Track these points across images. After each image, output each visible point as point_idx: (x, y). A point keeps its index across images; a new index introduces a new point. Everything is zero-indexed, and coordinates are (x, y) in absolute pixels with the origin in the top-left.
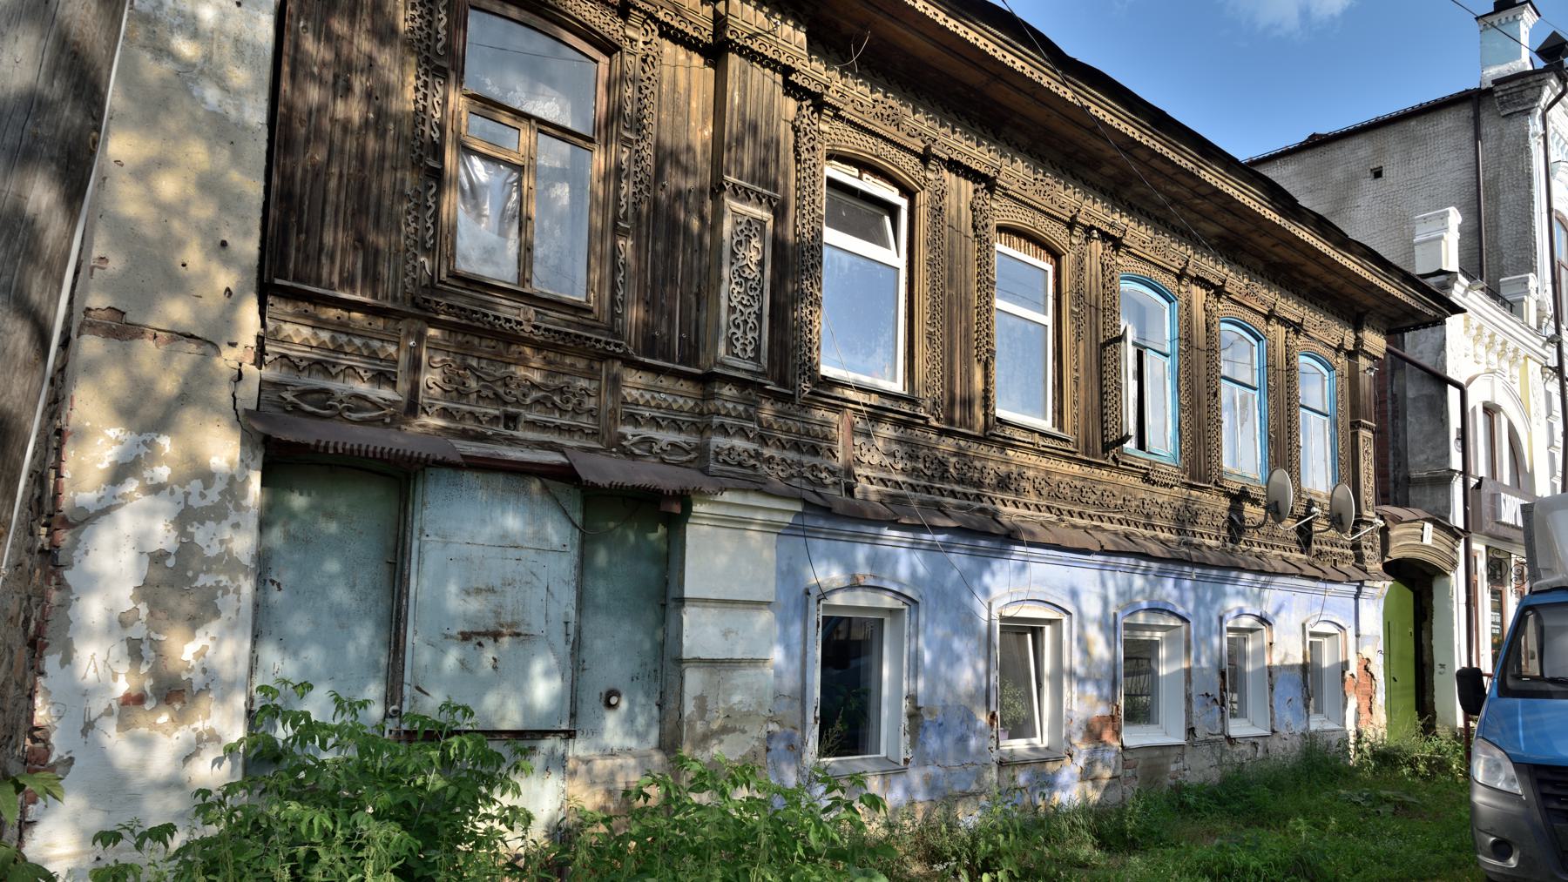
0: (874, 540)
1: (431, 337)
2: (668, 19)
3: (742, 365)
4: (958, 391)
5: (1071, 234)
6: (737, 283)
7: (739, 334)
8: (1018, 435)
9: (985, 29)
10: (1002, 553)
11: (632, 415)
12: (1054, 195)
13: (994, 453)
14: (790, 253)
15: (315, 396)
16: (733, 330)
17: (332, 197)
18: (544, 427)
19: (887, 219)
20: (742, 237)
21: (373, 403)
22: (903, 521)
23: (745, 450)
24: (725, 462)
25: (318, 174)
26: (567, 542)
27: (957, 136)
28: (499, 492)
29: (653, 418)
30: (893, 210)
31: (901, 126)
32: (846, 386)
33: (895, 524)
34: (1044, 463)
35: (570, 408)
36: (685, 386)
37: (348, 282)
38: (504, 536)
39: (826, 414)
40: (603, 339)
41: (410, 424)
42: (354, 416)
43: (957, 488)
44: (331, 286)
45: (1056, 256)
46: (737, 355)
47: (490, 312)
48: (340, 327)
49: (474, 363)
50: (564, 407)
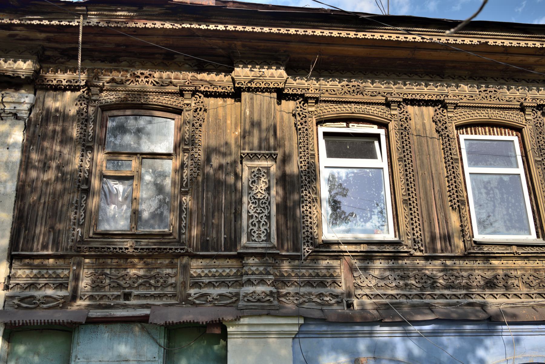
0: (371, 334)
1: (86, 263)
2: (207, 89)
3: (258, 245)
4: (437, 231)
5: (525, 114)
6: (253, 203)
7: (255, 229)
8: (495, 250)
9: (385, 29)
10: (491, 333)
11: (197, 283)
12: (498, 95)
13: (478, 264)
14: (295, 179)
15: (29, 299)
16: (251, 227)
17: (40, 213)
18: (145, 297)
19: (376, 143)
20: (256, 179)
21: (55, 298)
22: (386, 320)
23: (263, 292)
24: (248, 300)
25: (33, 206)
26: (156, 355)
27: (408, 86)
28: (118, 333)
29: (210, 282)
30: (377, 137)
31: (364, 93)
32: (338, 243)
33: (382, 323)
34: (531, 264)
35: (159, 284)
36: (230, 262)
37: (45, 247)
38: (119, 356)
39: (330, 261)
40: (173, 247)
41: (71, 306)
42: (45, 306)
43: (446, 292)
44: (37, 250)
45: (518, 130)
46: (255, 241)
47: (111, 247)
48: (40, 267)
49: (108, 272)
50: (157, 285)
